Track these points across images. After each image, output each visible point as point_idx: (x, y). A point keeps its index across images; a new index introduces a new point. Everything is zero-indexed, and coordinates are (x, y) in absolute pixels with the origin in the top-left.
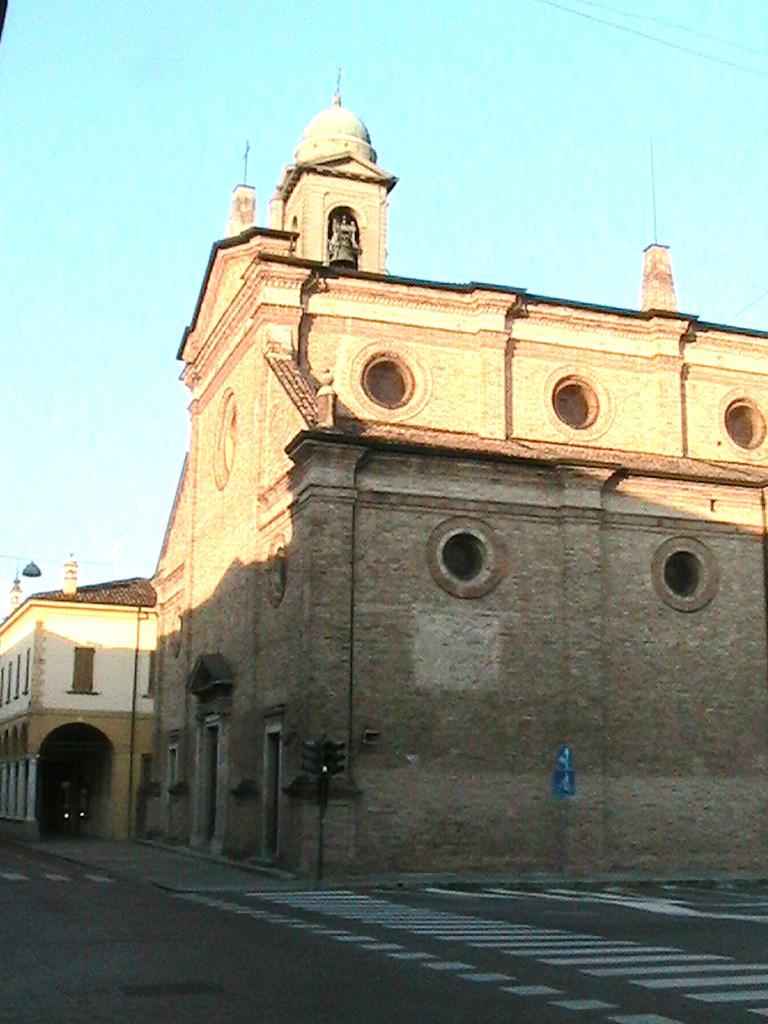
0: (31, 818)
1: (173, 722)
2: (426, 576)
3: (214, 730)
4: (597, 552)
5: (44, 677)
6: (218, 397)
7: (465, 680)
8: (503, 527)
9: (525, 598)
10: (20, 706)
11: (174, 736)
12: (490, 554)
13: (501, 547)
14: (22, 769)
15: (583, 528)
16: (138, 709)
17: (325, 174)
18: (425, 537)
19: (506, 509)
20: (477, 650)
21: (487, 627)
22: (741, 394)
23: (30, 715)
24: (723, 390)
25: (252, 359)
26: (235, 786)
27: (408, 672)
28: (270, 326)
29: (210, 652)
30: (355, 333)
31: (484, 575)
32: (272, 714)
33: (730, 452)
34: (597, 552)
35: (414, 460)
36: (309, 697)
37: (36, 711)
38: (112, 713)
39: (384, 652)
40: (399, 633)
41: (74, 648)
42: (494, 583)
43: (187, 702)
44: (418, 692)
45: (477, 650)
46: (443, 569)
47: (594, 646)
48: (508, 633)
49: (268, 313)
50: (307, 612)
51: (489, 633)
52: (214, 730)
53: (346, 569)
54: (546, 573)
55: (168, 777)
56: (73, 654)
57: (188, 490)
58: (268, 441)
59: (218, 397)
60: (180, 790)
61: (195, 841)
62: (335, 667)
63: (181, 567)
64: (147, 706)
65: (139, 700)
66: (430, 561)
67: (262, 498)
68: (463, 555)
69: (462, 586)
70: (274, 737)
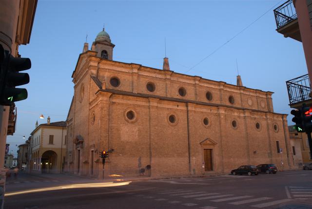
0: (40, 170)
1: (70, 149)
2: (123, 119)
3: (79, 150)
4: (156, 114)
5: (73, 85)
6: (80, 85)
7: (5, 139)
8: (138, 109)
9: (143, 123)
10: (38, 147)
11: (70, 152)
12: (136, 115)
13: (138, 113)
14: (38, 160)
15: (154, 110)
16: (102, 165)
17: (102, 44)
18: (123, 111)
19: (139, 106)
20: (133, 133)
21: (135, 129)
22: (181, 86)
23: (40, 149)
24: (178, 85)
25: (88, 77)
26: (84, 162)
27: (120, 138)
28: (92, 70)
29: (78, 135)
30: (109, 72)
31: (134, 119)
32: (91, 147)
33: (179, 97)
34: (156, 114)
35: (121, 96)
36: (100, 143)
37: (41, 148)
38: (15, 122)
39: (115, 134)
40: (118, 130)
41: (49, 135)
42: (137, 120)
43: (73, 145)
44: (121, 142)
45: (133, 133)
46: (126, 117)
47: (156, 132)
48: (139, 130)
49: (91, 68)
50: (100, 126)
51: (135, 130)
52: (79, 150)
53: (108, 117)
54: (146, 119)
55: (68, 161)
56: (49, 137)
57: (74, 103)
58: (91, 92)
59: (80, 85)
60: (71, 163)
61: (75, 173)
62: (106, 137)
63: (72, 119)
64: (64, 147)
65: (63, 146)
66: (124, 115)
67: (90, 104)
68: (131, 115)
69: (130, 121)
70: (93, 151)
